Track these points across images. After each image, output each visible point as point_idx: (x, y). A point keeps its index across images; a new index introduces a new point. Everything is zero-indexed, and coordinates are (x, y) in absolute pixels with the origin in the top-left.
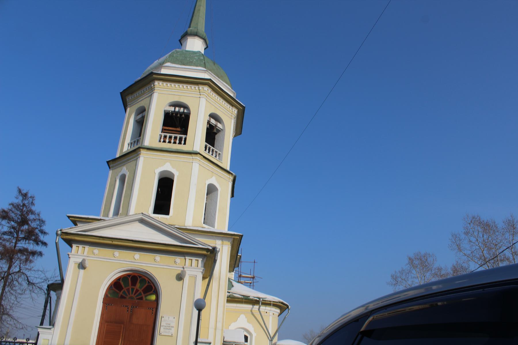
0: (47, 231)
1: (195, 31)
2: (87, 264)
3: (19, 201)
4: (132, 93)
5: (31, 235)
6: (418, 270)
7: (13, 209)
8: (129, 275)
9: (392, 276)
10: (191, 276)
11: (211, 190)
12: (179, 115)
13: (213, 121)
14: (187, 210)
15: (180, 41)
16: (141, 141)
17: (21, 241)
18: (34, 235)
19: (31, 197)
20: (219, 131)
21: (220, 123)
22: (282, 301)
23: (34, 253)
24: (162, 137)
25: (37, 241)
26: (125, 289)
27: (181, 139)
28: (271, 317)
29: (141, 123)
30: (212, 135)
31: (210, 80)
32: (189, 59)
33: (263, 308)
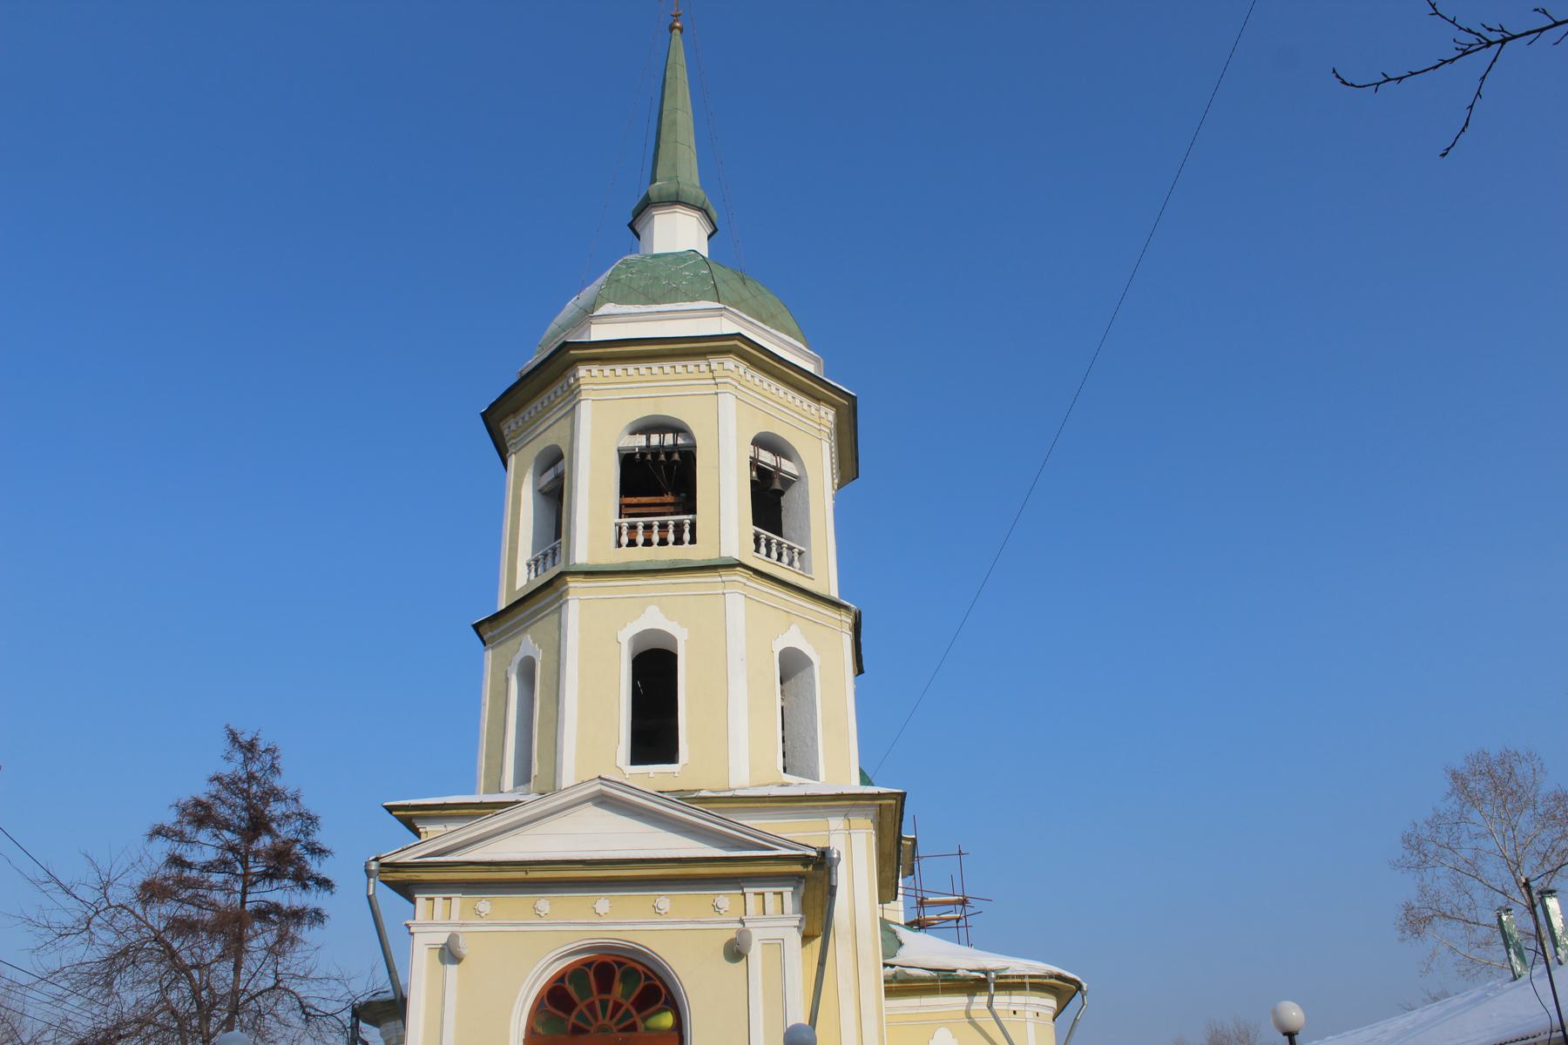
0: (326, 845)
1: (672, 188)
2: (465, 946)
3: (233, 767)
4: (515, 411)
5: (286, 864)
6: (1488, 809)
7: (224, 795)
8: (587, 964)
9: (1406, 840)
10: (767, 943)
11: (792, 666)
12: (662, 457)
13: (766, 457)
14: (729, 737)
15: (631, 226)
16: (563, 550)
17: (260, 884)
18: (291, 863)
19: (267, 750)
20: (788, 482)
21: (788, 458)
22: (1056, 970)
23: (297, 915)
24: (625, 532)
25: (303, 879)
26: (581, 1006)
27: (679, 527)
28: (1030, 1026)
29: (555, 496)
30: (769, 499)
31: (739, 336)
32: (667, 280)
33: (1002, 1000)
